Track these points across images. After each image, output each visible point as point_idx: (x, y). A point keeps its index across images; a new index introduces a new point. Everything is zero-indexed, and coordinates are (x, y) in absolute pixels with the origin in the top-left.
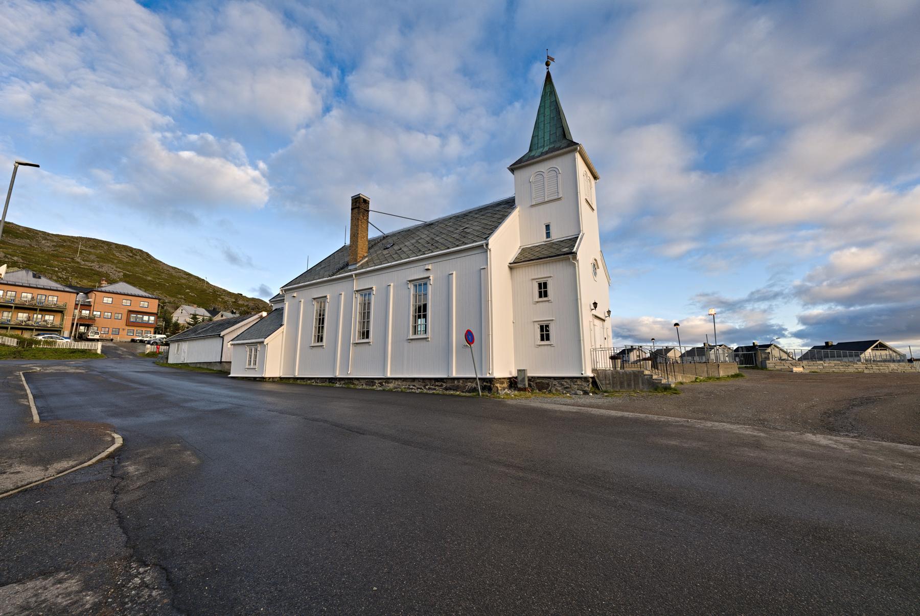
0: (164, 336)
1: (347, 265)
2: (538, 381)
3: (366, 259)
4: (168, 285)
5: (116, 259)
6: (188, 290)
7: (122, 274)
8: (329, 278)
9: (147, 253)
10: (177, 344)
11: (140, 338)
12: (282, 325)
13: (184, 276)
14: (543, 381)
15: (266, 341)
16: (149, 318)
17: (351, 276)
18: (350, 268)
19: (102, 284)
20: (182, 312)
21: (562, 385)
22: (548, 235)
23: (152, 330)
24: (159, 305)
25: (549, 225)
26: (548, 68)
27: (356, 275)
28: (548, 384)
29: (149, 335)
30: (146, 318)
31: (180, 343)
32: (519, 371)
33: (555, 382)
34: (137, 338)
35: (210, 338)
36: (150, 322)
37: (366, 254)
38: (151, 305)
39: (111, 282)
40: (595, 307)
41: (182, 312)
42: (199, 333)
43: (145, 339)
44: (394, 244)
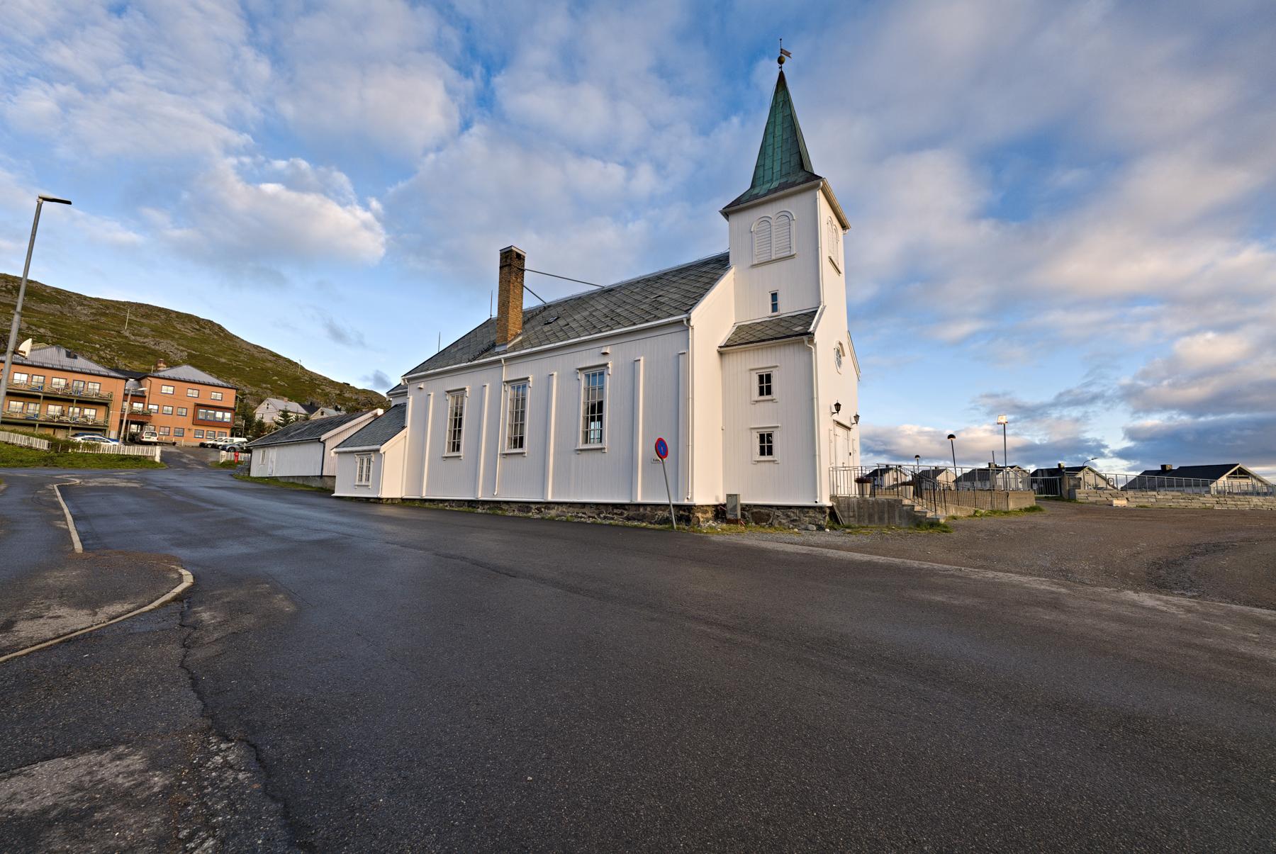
0: (245, 440)
1: (494, 345)
2: (755, 510)
3: (520, 338)
4: (248, 369)
5: (177, 334)
6: (276, 378)
7: (186, 354)
8: (469, 363)
9: (219, 325)
10: (261, 451)
11: (212, 442)
12: (404, 427)
13: (270, 358)
14: (762, 511)
15: (383, 448)
16: (223, 415)
17: (499, 361)
18: (497, 349)
19: (159, 367)
20: (268, 408)
21: (788, 516)
22: (775, 307)
23: (228, 431)
24: (237, 397)
25: (776, 294)
26: (781, 67)
27: (506, 360)
28: (768, 515)
29: (224, 438)
30: (219, 415)
31: (266, 449)
32: (729, 496)
33: (779, 513)
34: (209, 442)
35: (299, 444)
36: (225, 420)
37: (519, 331)
38: (227, 397)
39: (172, 364)
40: (838, 410)
41: (268, 408)
42: (292, 437)
43: (219, 443)
44: (558, 318)
